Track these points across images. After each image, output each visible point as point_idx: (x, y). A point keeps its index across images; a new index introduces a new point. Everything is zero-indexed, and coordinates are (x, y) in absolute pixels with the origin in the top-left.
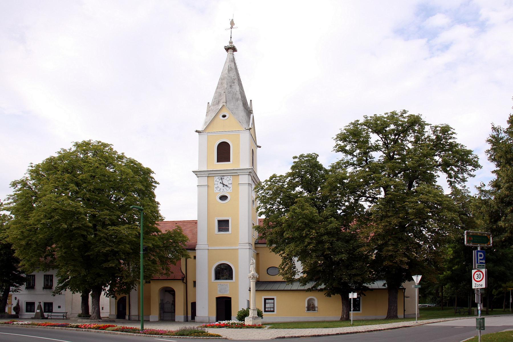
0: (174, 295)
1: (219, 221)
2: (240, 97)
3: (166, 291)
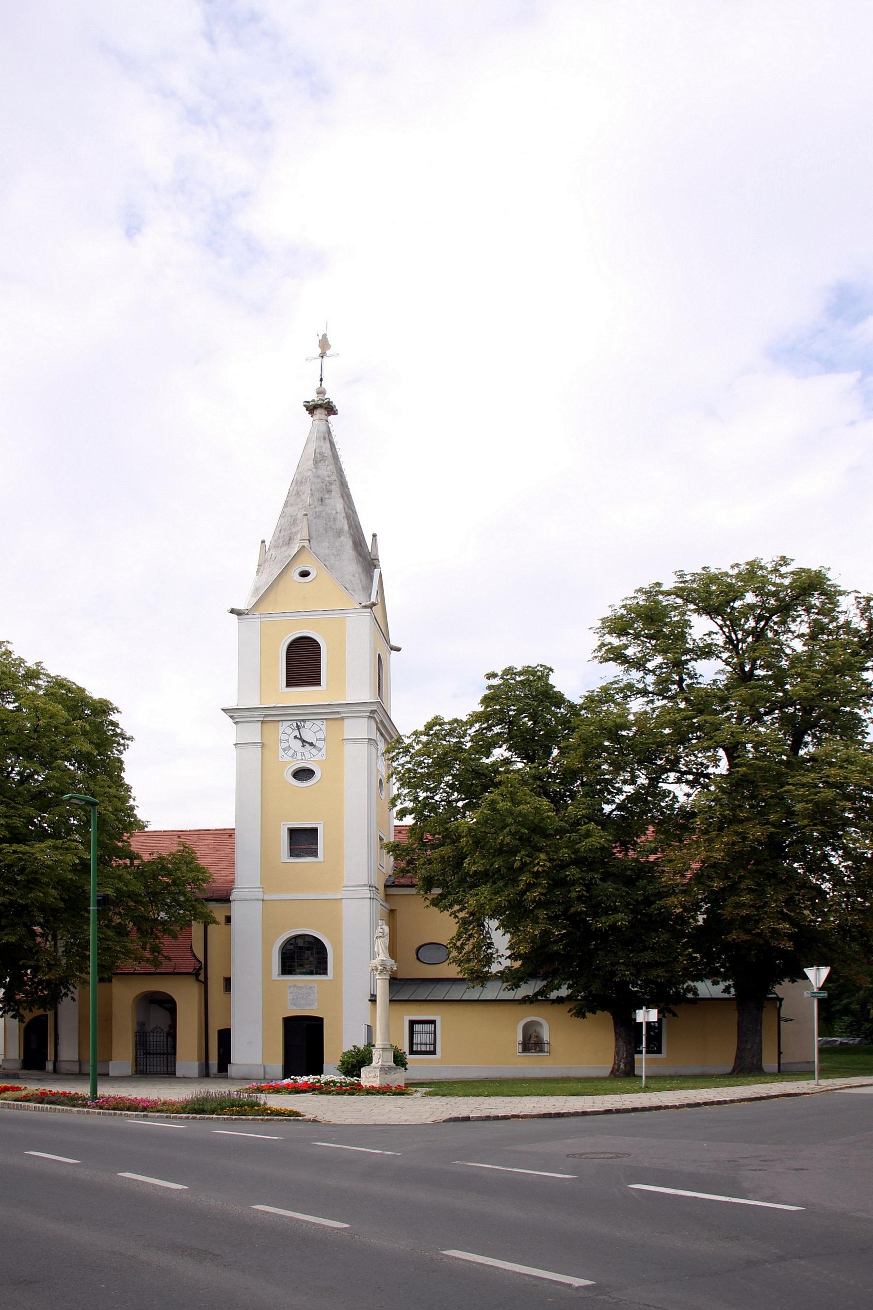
1: (293, 832)
2: (346, 527)
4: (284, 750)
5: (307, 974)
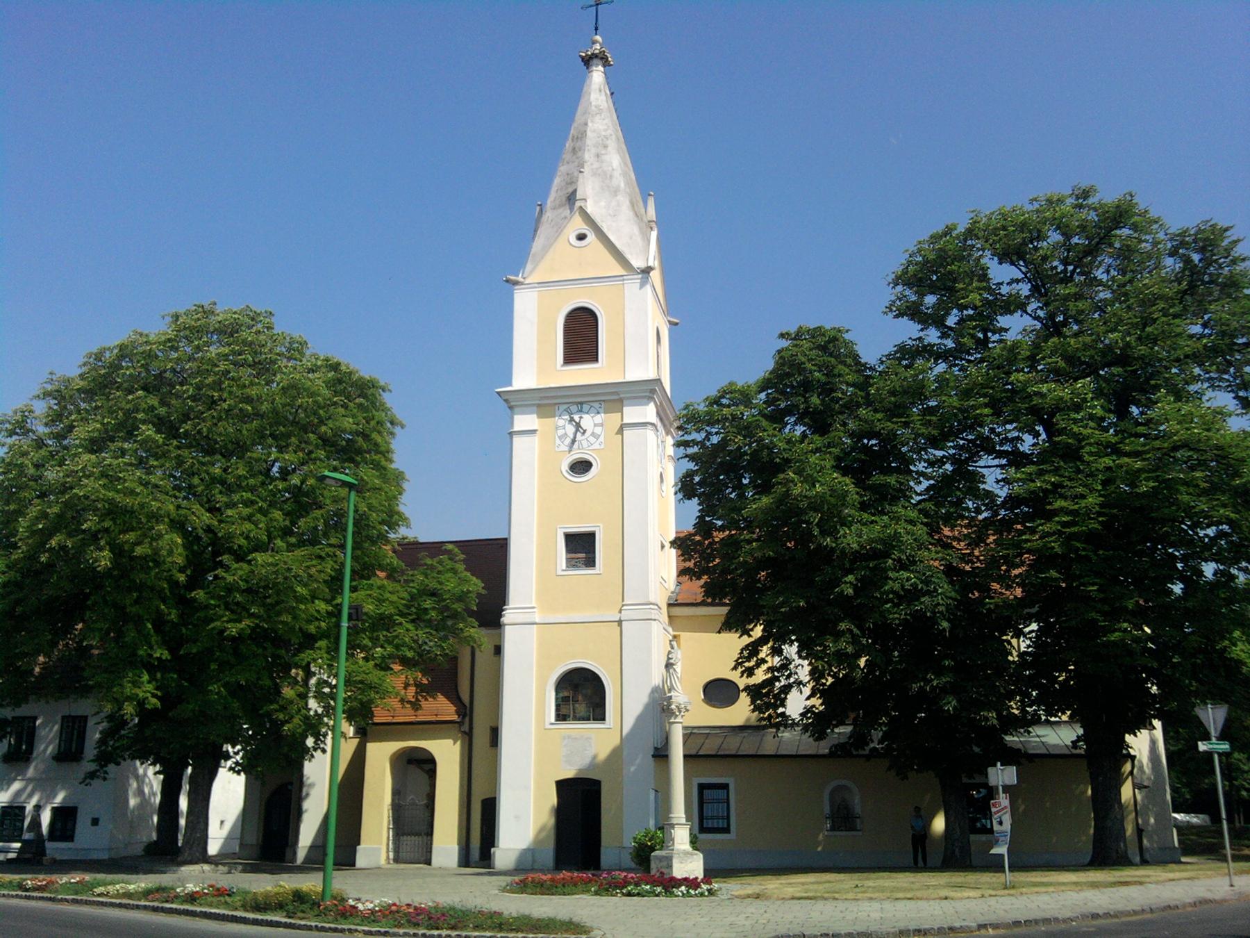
0: (432, 773)
2: (622, 185)
3: (410, 762)
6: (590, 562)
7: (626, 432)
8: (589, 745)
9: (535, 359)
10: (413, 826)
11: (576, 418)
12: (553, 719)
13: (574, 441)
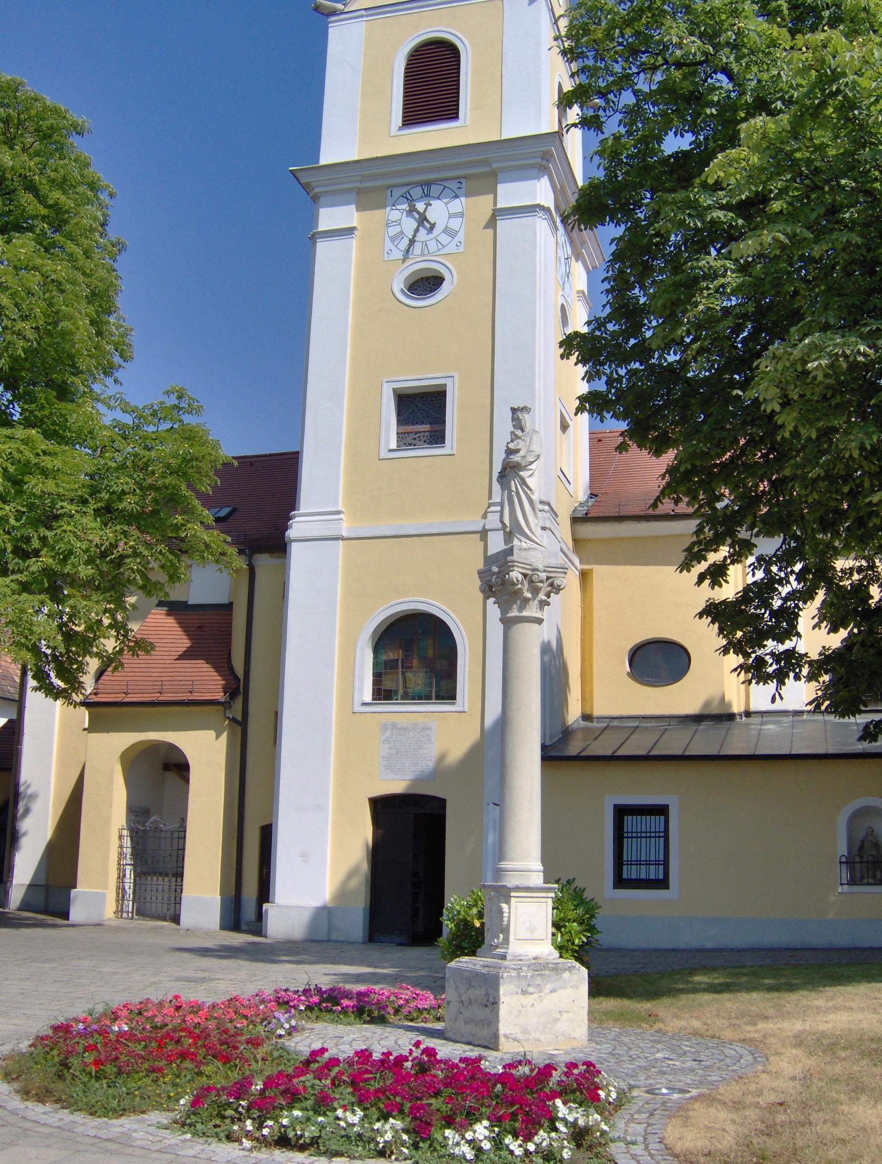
4: (392, 239)
5: (420, 698)
6: (437, 438)
7: (502, 225)
8: (431, 739)
9: (358, 110)
10: (156, 857)
11: (420, 206)
12: (368, 697)
13: (412, 242)
